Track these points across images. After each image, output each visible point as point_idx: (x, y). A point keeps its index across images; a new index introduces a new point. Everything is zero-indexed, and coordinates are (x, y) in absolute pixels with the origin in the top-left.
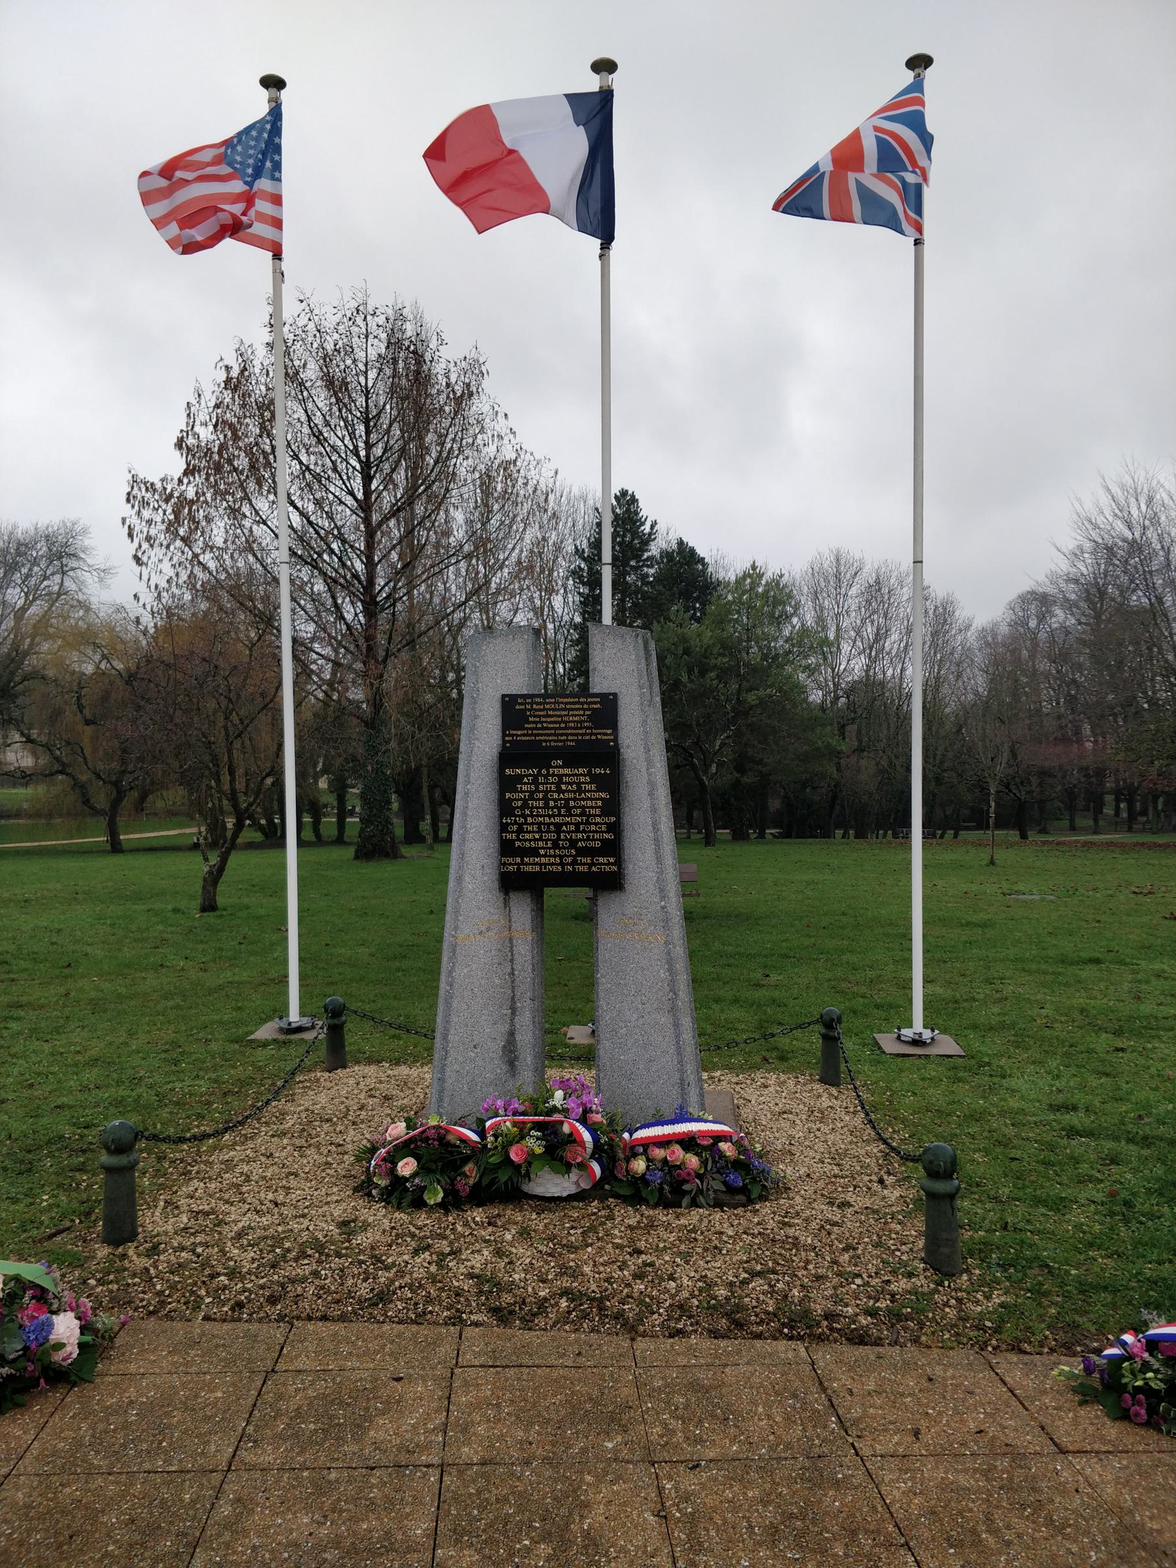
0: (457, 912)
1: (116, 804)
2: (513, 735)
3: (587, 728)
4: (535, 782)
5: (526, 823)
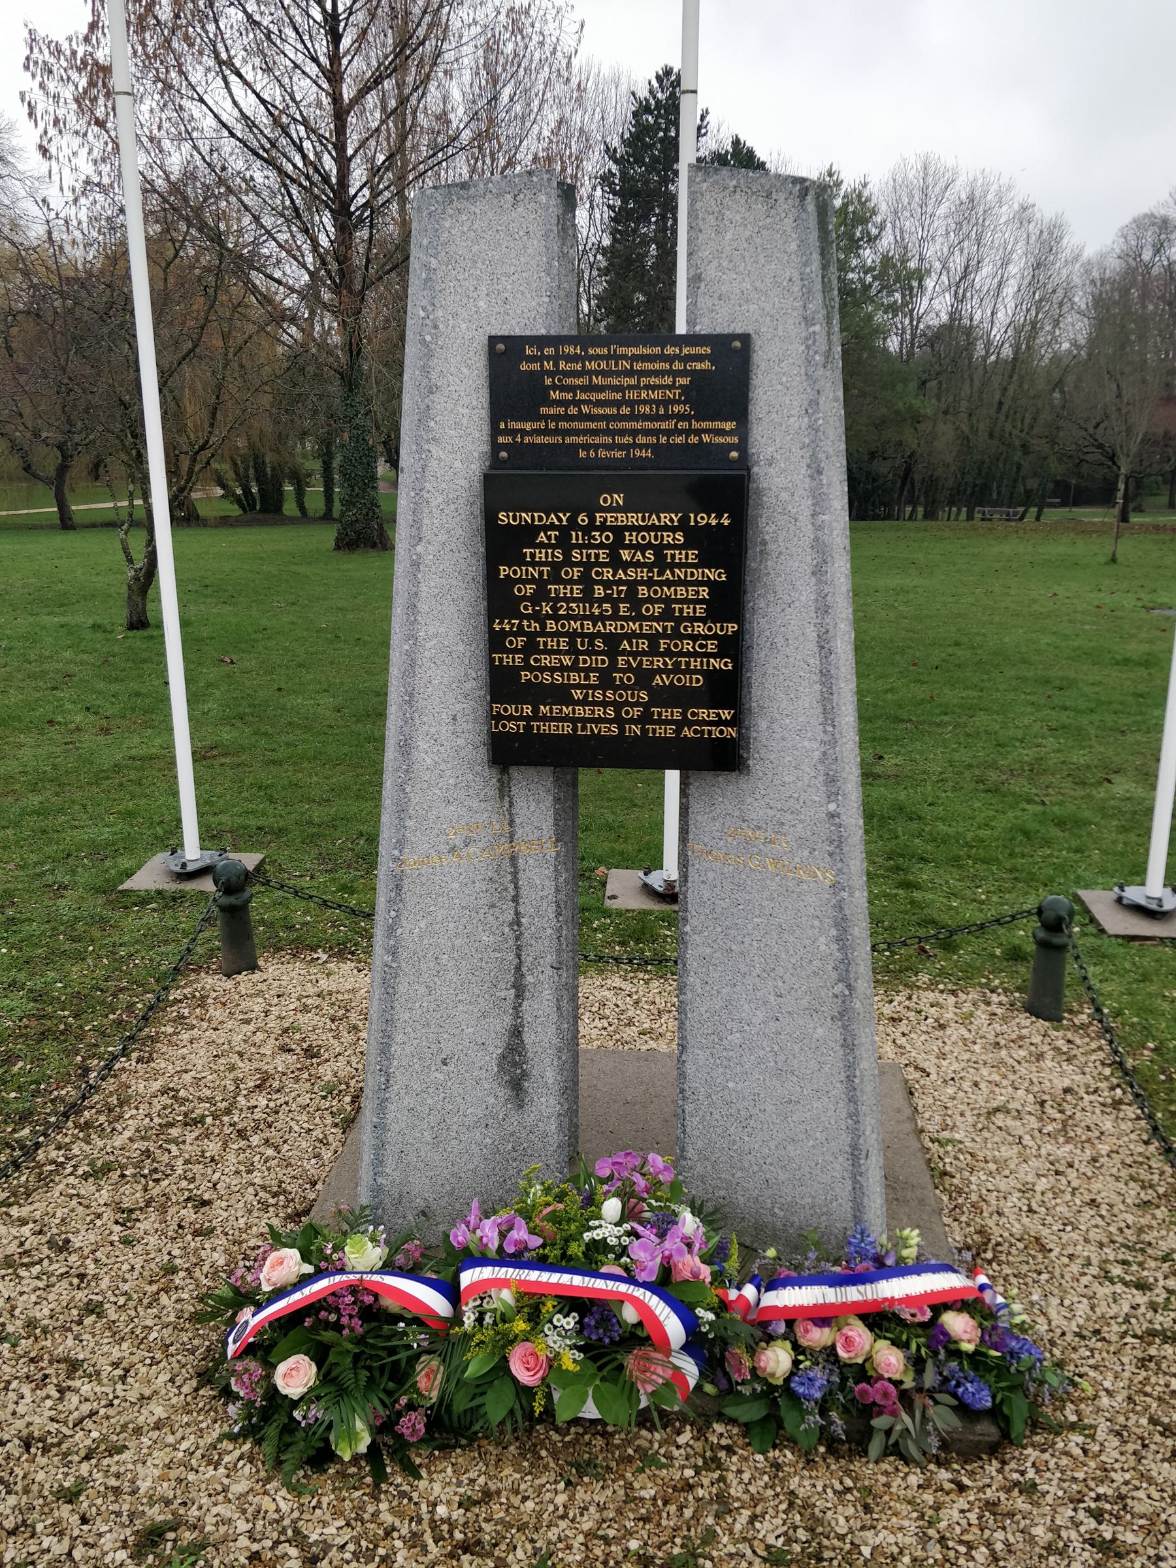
0: (401, 812)
1: (63, 469)
2: (513, 432)
3: (681, 417)
4: (563, 542)
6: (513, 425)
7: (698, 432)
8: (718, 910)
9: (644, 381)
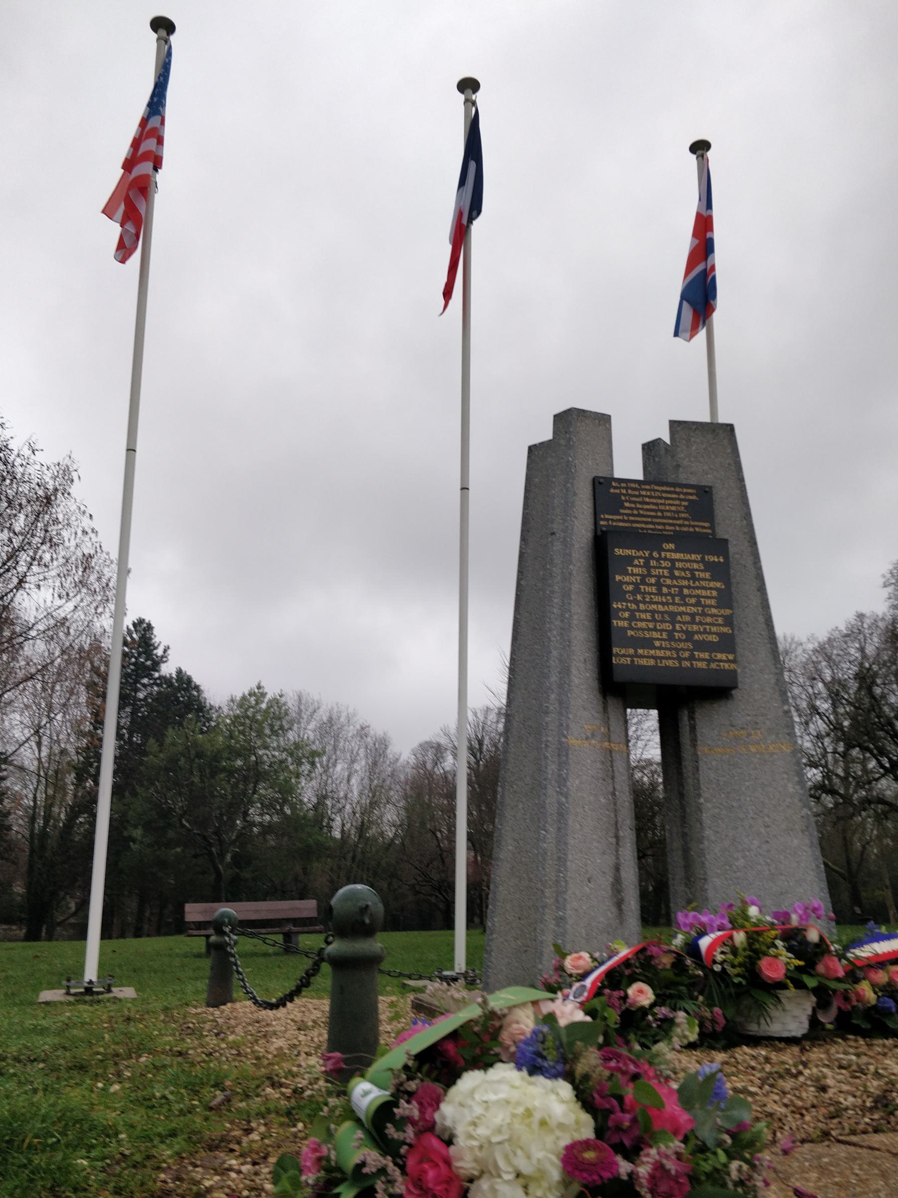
2: (608, 520)
3: (685, 519)
4: (647, 565)
5: (639, 611)
6: (607, 516)
7: (693, 526)
8: (721, 783)
9: (668, 502)
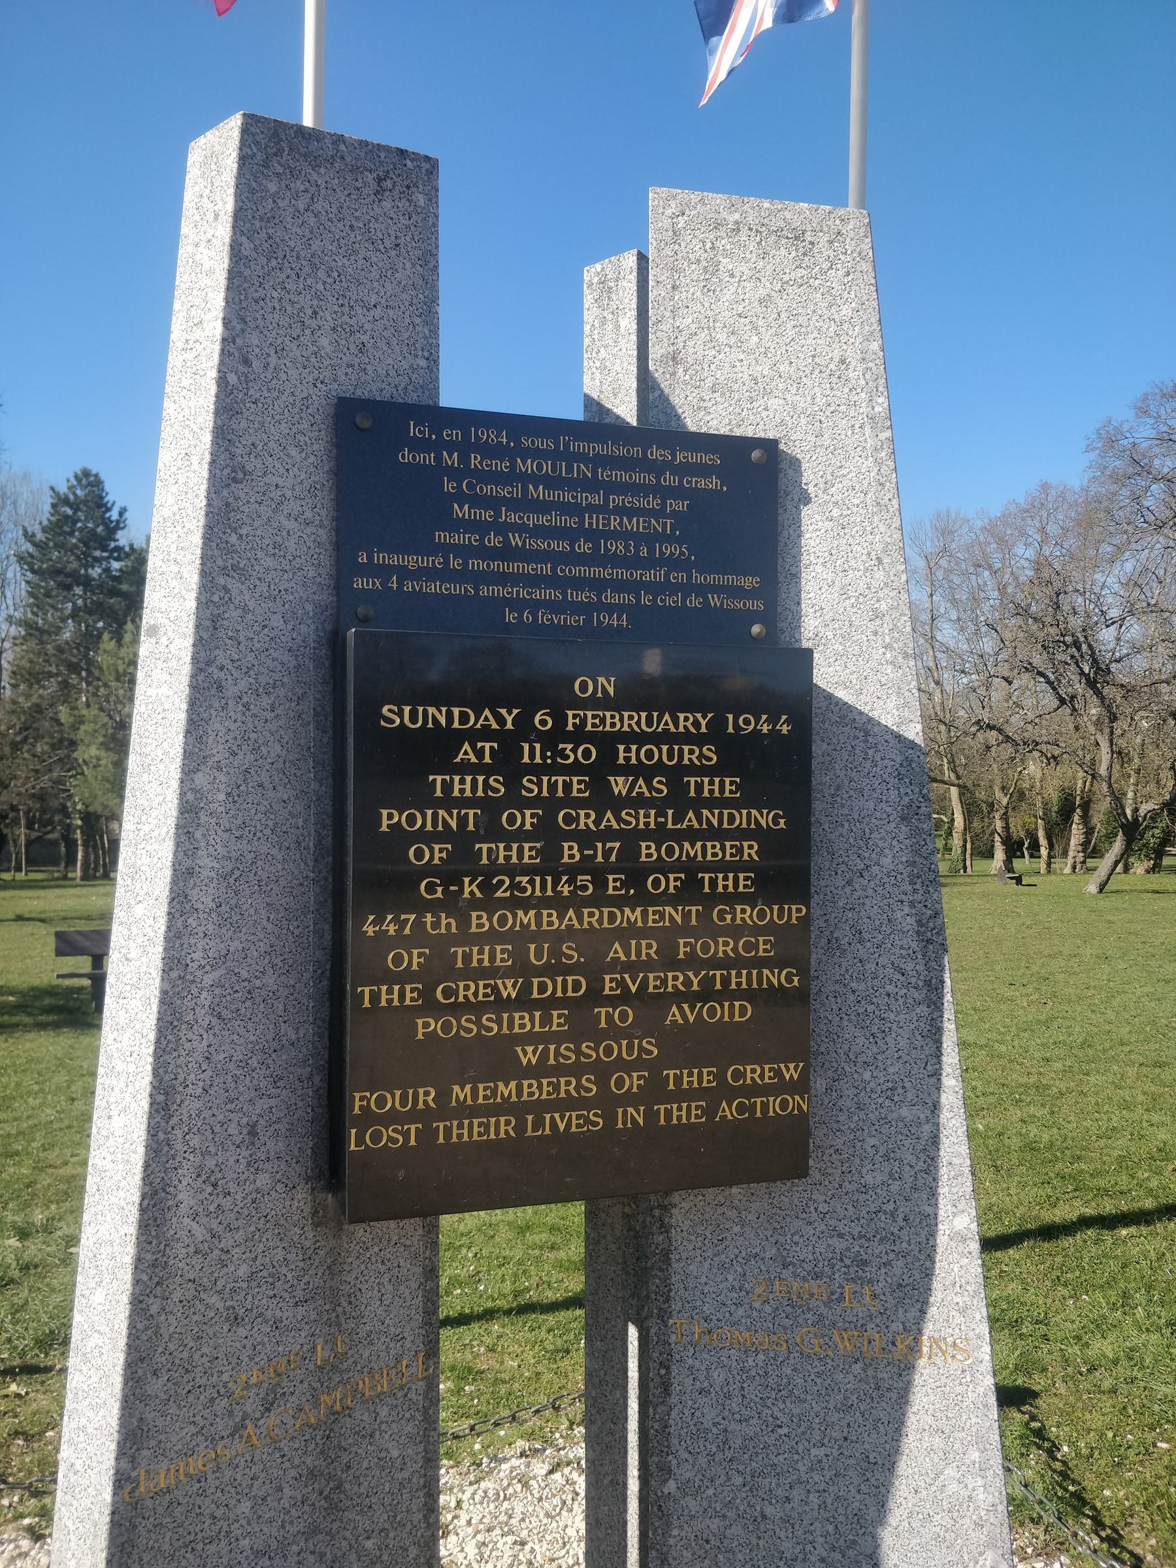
2: (384, 572)
3: (673, 564)
5: (465, 937)
6: (380, 558)
7: (702, 590)
9: (615, 500)
